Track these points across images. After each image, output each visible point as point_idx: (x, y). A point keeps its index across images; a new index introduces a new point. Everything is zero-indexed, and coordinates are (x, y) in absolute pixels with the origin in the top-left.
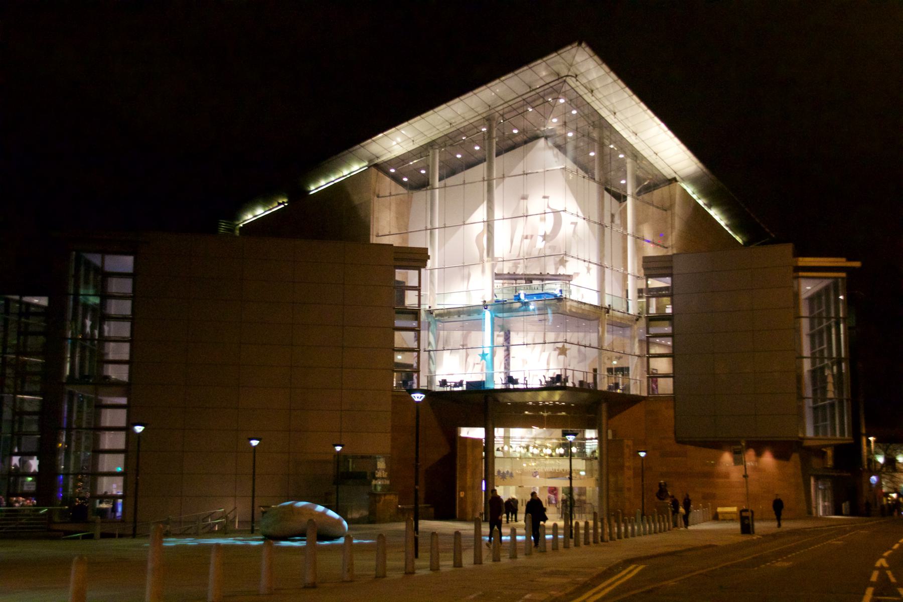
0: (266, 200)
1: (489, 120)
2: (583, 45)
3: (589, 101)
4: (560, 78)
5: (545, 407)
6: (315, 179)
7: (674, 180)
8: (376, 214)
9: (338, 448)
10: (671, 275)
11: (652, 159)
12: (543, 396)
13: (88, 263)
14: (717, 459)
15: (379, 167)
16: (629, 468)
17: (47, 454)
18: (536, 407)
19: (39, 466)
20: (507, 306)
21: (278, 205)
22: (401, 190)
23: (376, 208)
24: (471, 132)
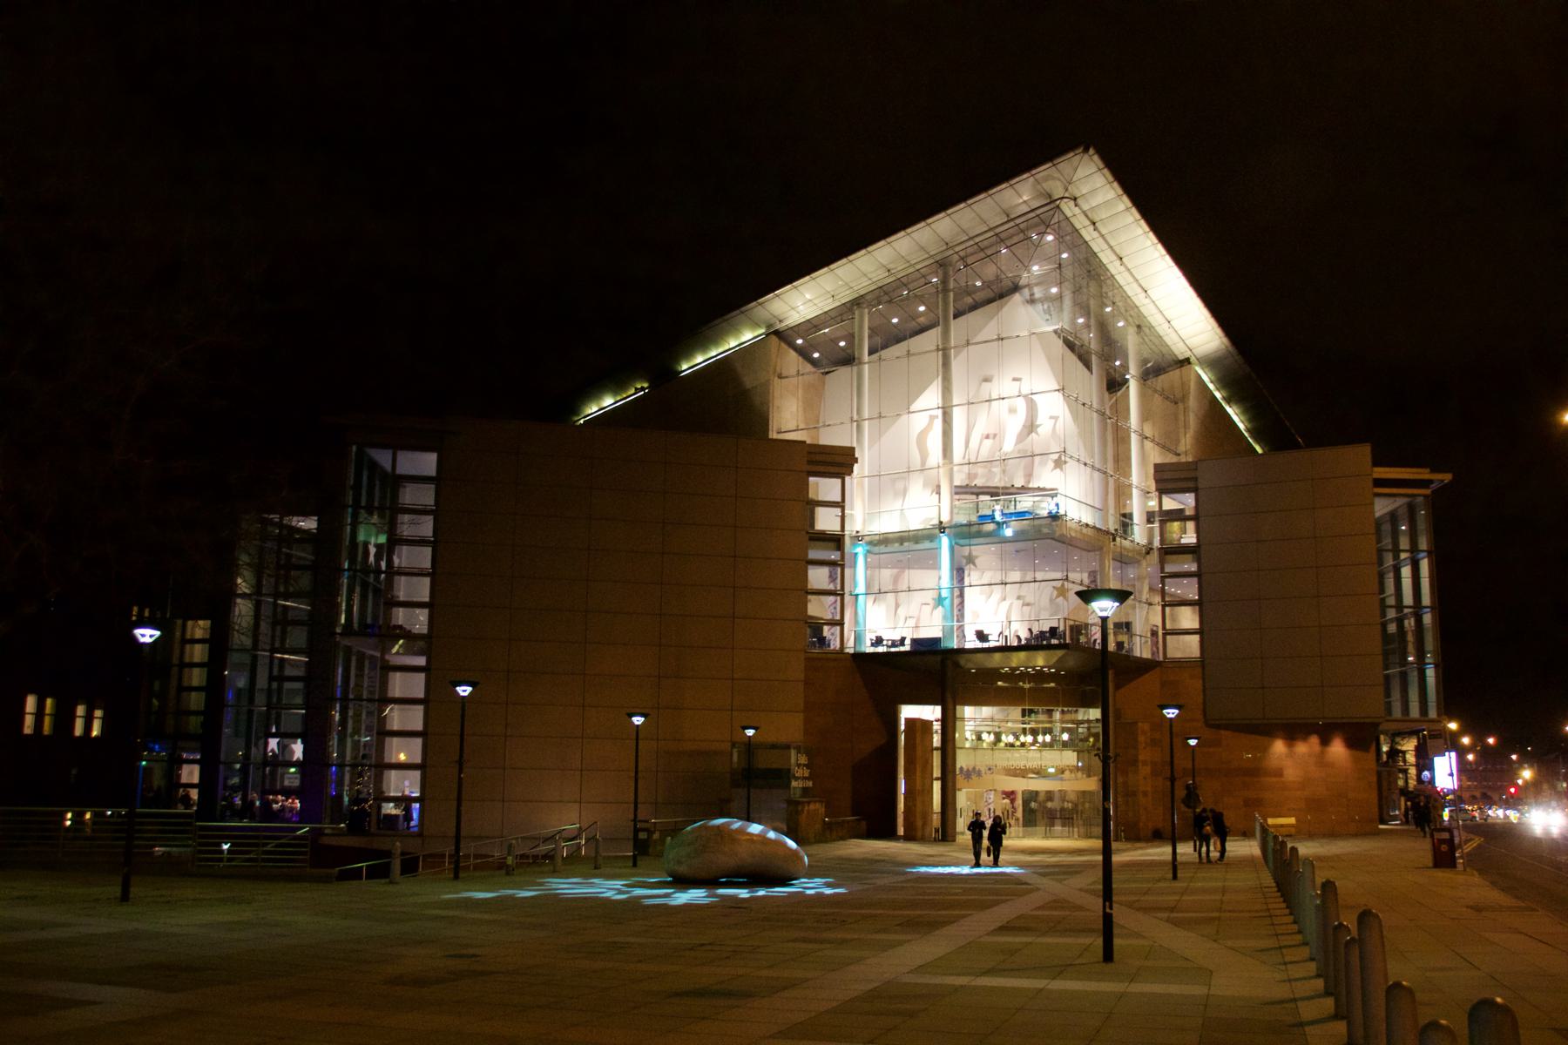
0: (617, 386)
1: (942, 265)
2: (1091, 151)
3: (1087, 238)
4: (1052, 203)
5: (1024, 676)
6: (688, 354)
7: (1187, 361)
8: (777, 402)
9: (750, 732)
10: (1195, 490)
11: (1163, 329)
12: (1018, 659)
13: (374, 466)
14: (1265, 749)
15: (781, 335)
16: (1145, 763)
17: (315, 738)
18: (1013, 676)
19: (304, 753)
20: (974, 529)
21: (636, 391)
22: (809, 368)
23: (777, 394)
24: (916, 284)
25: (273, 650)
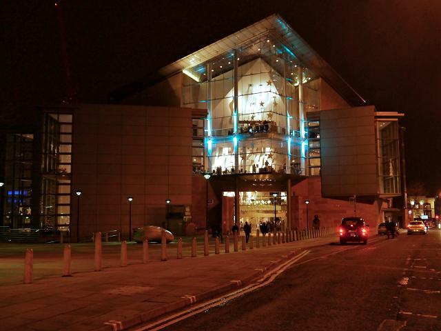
9: (168, 202)
13: (52, 119)
19: (31, 212)
25: (20, 179)
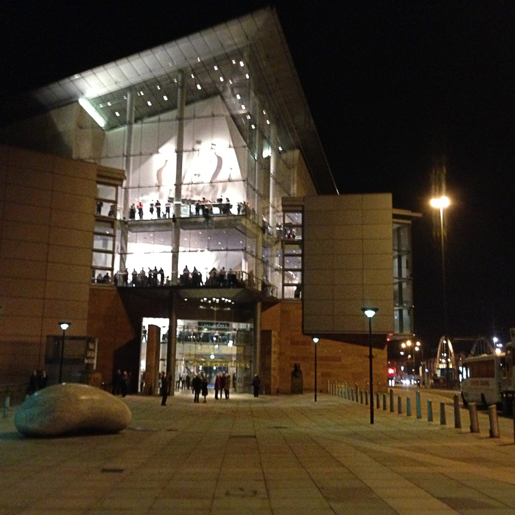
16: (275, 352)
